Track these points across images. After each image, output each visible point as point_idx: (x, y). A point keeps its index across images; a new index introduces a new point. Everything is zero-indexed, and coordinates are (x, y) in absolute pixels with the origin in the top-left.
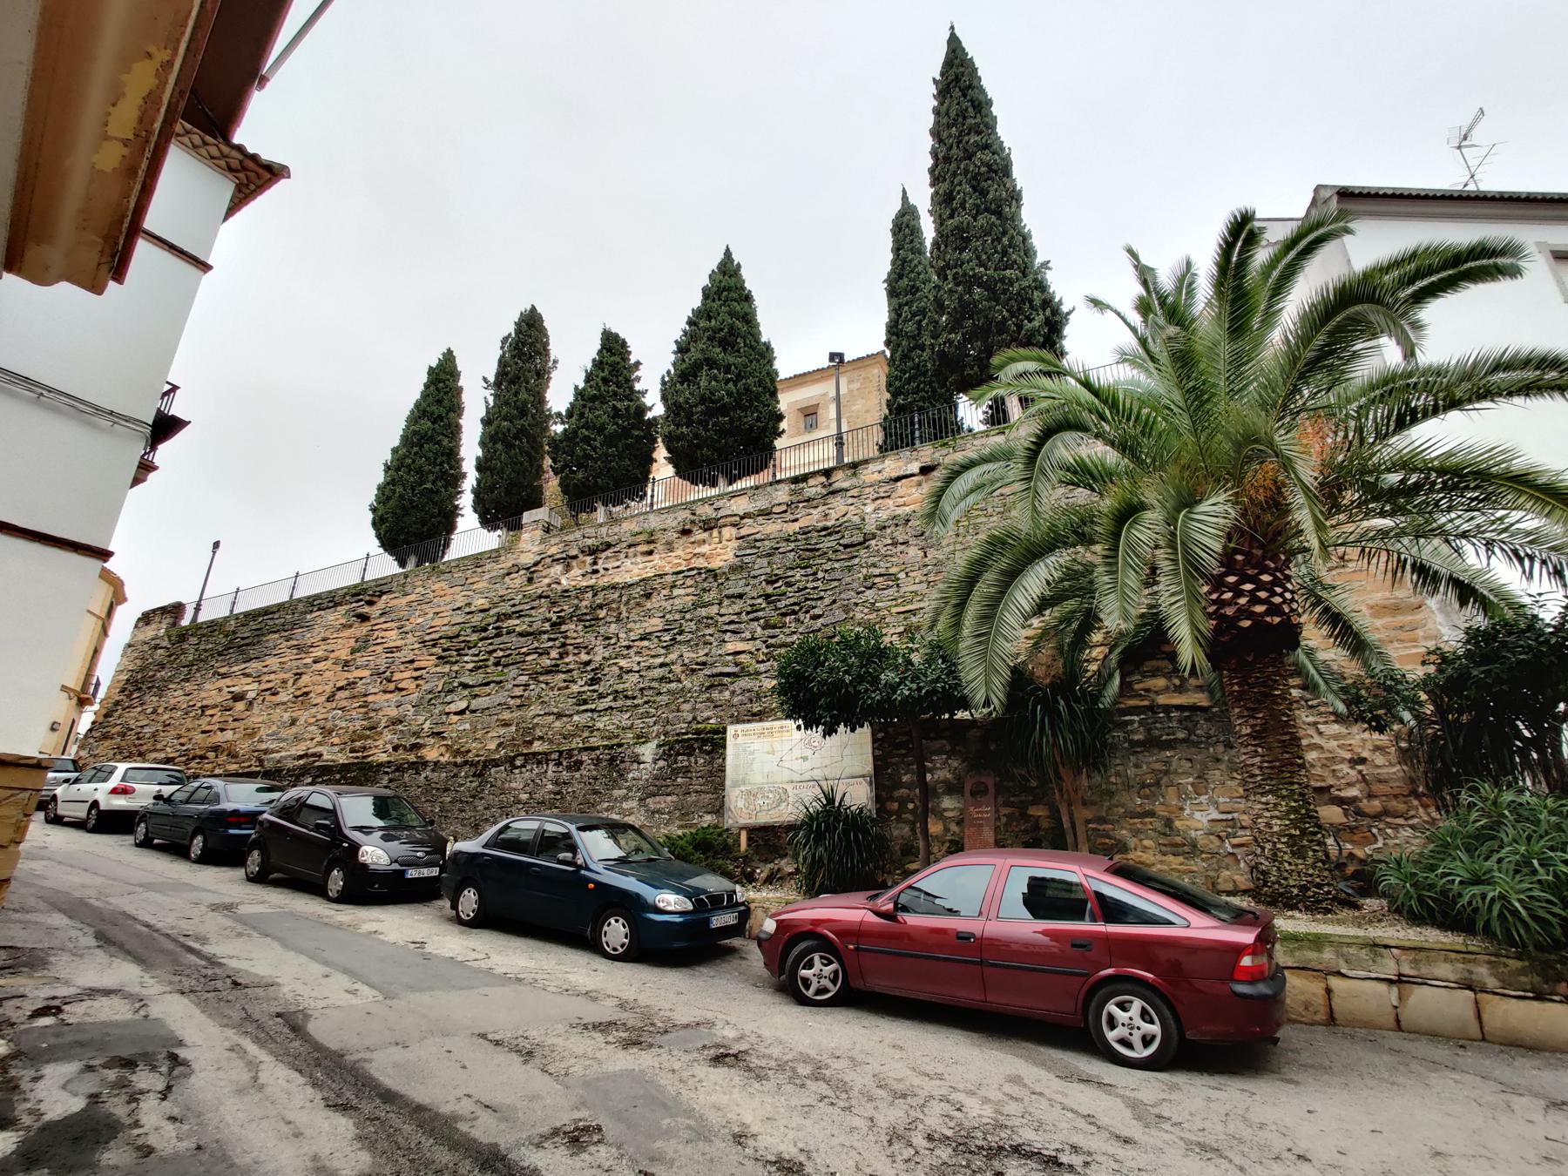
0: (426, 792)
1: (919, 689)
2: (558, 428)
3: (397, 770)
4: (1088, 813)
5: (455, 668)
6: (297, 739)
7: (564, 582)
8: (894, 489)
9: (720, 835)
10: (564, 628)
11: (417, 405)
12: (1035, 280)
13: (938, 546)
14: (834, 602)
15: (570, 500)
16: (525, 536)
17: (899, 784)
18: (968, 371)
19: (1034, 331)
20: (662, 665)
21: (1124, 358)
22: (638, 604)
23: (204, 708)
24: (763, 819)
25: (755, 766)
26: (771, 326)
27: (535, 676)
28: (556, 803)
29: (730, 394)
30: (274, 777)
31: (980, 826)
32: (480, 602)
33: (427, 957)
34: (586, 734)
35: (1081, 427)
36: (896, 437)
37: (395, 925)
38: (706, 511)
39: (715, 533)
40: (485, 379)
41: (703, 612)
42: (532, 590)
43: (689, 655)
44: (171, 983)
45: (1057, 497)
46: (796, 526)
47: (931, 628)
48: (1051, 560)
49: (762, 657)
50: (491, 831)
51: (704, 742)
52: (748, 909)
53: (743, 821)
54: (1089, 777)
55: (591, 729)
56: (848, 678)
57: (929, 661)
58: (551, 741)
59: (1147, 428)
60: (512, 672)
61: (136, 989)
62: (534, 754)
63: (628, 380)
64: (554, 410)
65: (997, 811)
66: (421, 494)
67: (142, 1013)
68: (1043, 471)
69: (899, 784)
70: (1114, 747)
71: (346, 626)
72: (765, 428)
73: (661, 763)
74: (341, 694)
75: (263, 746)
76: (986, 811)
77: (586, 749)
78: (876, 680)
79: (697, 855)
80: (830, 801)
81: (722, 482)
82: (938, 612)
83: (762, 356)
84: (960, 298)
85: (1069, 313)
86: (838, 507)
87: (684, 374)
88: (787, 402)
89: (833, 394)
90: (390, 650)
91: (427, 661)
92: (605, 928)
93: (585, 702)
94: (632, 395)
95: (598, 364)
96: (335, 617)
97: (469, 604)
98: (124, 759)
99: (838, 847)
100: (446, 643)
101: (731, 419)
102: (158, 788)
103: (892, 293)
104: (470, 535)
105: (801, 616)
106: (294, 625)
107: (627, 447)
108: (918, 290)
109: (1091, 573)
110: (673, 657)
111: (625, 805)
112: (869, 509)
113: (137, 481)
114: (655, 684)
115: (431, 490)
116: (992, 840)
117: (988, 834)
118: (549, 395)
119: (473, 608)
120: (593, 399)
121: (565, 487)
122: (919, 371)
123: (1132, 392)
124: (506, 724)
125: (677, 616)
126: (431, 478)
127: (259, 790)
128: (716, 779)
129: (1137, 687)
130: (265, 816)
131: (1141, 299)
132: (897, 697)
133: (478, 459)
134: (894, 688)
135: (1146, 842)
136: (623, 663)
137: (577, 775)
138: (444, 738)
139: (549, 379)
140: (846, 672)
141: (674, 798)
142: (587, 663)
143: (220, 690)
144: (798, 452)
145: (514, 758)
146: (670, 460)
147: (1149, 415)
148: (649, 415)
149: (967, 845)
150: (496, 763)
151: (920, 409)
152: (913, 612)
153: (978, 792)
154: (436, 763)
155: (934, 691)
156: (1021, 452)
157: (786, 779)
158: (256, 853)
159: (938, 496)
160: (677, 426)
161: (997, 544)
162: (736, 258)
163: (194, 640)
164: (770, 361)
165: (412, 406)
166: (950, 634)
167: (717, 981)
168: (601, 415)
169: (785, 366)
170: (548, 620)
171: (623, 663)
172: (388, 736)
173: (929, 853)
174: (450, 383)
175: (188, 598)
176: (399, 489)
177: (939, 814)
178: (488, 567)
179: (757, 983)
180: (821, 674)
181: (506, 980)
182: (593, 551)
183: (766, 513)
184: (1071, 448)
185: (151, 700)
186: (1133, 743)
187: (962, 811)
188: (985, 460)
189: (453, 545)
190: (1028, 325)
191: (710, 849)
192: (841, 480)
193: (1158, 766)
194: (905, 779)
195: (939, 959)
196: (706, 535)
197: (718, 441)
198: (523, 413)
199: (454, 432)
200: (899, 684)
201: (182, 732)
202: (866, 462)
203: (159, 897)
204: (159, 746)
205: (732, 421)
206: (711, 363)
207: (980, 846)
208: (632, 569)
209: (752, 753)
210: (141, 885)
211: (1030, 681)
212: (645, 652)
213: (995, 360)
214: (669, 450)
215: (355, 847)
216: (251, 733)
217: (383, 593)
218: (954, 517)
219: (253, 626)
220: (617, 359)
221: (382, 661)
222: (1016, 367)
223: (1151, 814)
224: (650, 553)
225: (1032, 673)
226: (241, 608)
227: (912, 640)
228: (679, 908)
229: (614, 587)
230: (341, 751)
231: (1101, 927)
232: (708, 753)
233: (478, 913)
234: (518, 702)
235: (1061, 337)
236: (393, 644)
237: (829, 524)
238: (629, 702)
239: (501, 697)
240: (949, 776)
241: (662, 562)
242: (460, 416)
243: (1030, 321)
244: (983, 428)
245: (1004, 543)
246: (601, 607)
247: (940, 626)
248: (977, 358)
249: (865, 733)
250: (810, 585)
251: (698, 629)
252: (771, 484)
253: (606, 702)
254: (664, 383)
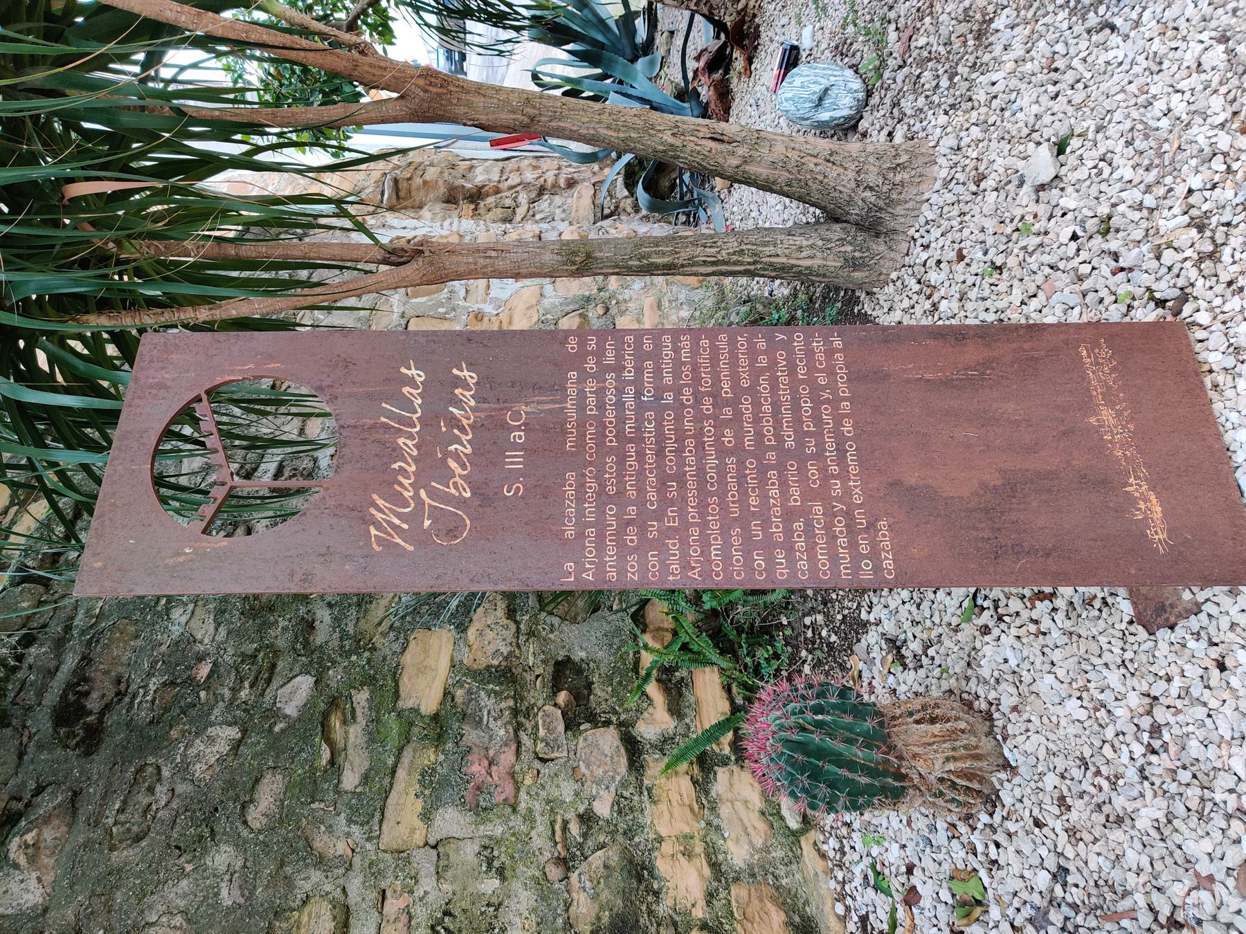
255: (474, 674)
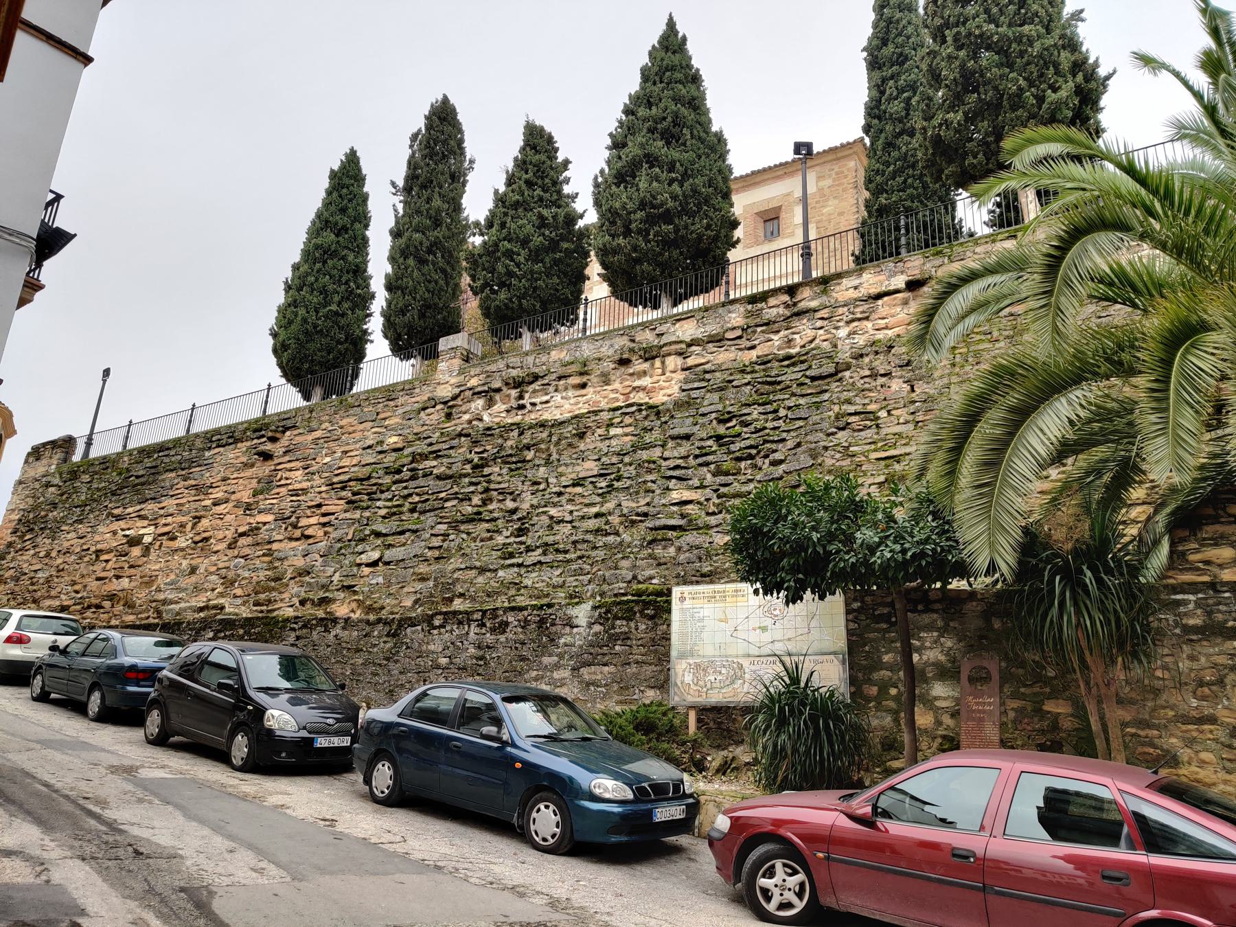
0: (337, 652)
1: (904, 551)
2: (477, 240)
3: (304, 626)
4: (1124, 714)
5: (367, 514)
6: (197, 589)
7: (486, 418)
8: (876, 309)
9: (665, 714)
10: (486, 471)
11: (319, 215)
12: (1062, 37)
13: (928, 378)
14: (799, 445)
15: (492, 324)
16: (442, 366)
17: (878, 665)
18: (970, 160)
19: (1059, 105)
20: (597, 515)
21: (1182, 132)
22: (570, 445)
23: (98, 553)
24: (715, 698)
25: (705, 635)
26: (725, 111)
27: (455, 525)
28: (478, 669)
29: (674, 197)
30: (173, 630)
31: (981, 720)
32: (393, 440)
33: (339, 837)
34: (512, 592)
35: (1121, 226)
36: (876, 246)
37: (303, 798)
38: (647, 337)
39: (658, 363)
40: (393, 184)
41: (644, 455)
42: (450, 426)
43: (628, 504)
44: (72, 847)
45: (1084, 316)
46: (753, 355)
47: (919, 477)
48: (1077, 394)
49: (712, 509)
50: (406, 699)
51: (646, 604)
52: (698, 802)
53: (691, 699)
54: (1125, 667)
55: (518, 586)
56: (815, 536)
57: (916, 518)
58: (473, 599)
59: (1213, 225)
60: (430, 519)
61: (37, 852)
62: (455, 613)
63: (555, 183)
64: (472, 219)
65: (1003, 704)
66: (326, 317)
67: (44, 878)
68: (1068, 283)
69: (878, 665)
70: (1160, 632)
71: (247, 465)
72: (716, 239)
73: (597, 628)
74: (243, 541)
75: (161, 596)
76: (988, 703)
77: (513, 609)
78: (849, 539)
79: (639, 736)
80: (795, 680)
81: (665, 303)
82: (927, 458)
83: (713, 149)
84: (963, 66)
85: (1108, 78)
86: (804, 331)
87: (621, 174)
88: (742, 204)
89: (798, 193)
90: (295, 493)
91: (336, 506)
92: (534, 814)
93: (511, 555)
94: (560, 200)
95: (521, 164)
96: (235, 454)
97: (381, 443)
98: (19, 606)
99: (811, 737)
100: (356, 486)
101: (676, 227)
102: (54, 637)
103: (874, 64)
104: (381, 366)
105: (759, 461)
106: (191, 462)
107: (556, 262)
108: (907, 59)
109: (1131, 412)
110: (610, 505)
111: (556, 675)
112: (843, 333)
113: (22, 302)
114: (590, 537)
115: (336, 313)
116: (996, 739)
117: (992, 732)
118: (465, 201)
119: (385, 447)
120: (516, 205)
121: (486, 312)
122: (908, 163)
123: (1192, 178)
124: (423, 579)
125: (615, 459)
126: (336, 298)
127: (157, 644)
128: (660, 648)
129: (1192, 557)
130: (165, 672)
131: (1208, 54)
132: (876, 559)
133: (387, 276)
134: (872, 549)
135: (1205, 756)
136: (553, 512)
137: (502, 638)
138: (355, 593)
139: (464, 184)
140: (813, 528)
141: (611, 669)
142: (513, 511)
143: (114, 533)
144: (755, 266)
145: (432, 616)
146: (605, 278)
147: (1216, 207)
148: (581, 223)
149: (963, 744)
150: (412, 623)
151: (907, 209)
152: (897, 459)
153: (979, 678)
154: (347, 620)
155: (923, 554)
156: (1039, 260)
157: (741, 652)
158: (155, 713)
159: (929, 316)
160: (613, 236)
161: (1003, 376)
162: (681, 29)
163: (86, 478)
164: (723, 156)
165: (313, 216)
166: (943, 484)
167: (661, 884)
168: (524, 224)
169: (740, 162)
170: (470, 461)
171: (553, 512)
172: (294, 588)
173: (916, 749)
174: (355, 189)
175: (79, 431)
176: (302, 312)
177: (929, 703)
178: (400, 401)
179: (707, 890)
180: (784, 530)
181: (423, 867)
182: (518, 384)
183: (717, 340)
184: (1102, 254)
185: (44, 542)
186: (1187, 629)
187: (958, 701)
188: (989, 271)
189: (363, 374)
190: (1051, 96)
191: (652, 730)
192: (807, 298)
193: (1222, 660)
194: (886, 658)
195: (929, 879)
196: (646, 365)
197: (661, 254)
198: (437, 223)
199: (362, 245)
200: (879, 544)
201: (76, 578)
202: (839, 276)
203: (58, 756)
204: (53, 593)
205: (677, 230)
206: (652, 160)
207: (983, 745)
208: (561, 405)
209: (701, 620)
210: (38, 742)
211: (1046, 546)
212: (579, 500)
213: (1007, 144)
214: (604, 264)
215: (260, 711)
216: (149, 581)
217: (286, 429)
218: (949, 342)
219: (148, 462)
220: (543, 157)
221: (287, 504)
222: (1033, 148)
223: (1212, 720)
224: (584, 386)
225: (1050, 536)
226: (133, 444)
227: (895, 492)
228: (619, 797)
229: (542, 425)
230: (244, 604)
231: (1141, 857)
232: (651, 618)
233: (392, 790)
234: (437, 553)
235: (1098, 110)
236: (298, 486)
237: (793, 351)
238: (560, 557)
239: (418, 548)
240: (942, 658)
241: (598, 397)
242: (366, 226)
243: (1055, 90)
244: (988, 230)
245: (1013, 374)
246: (528, 448)
247: (930, 476)
248: (984, 143)
249: (836, 602)
250: (770, 425)
251: (638, 475)
252: (723, 305)
253: (535, 556)
254: (597, 185)
255: (1056, 719)
